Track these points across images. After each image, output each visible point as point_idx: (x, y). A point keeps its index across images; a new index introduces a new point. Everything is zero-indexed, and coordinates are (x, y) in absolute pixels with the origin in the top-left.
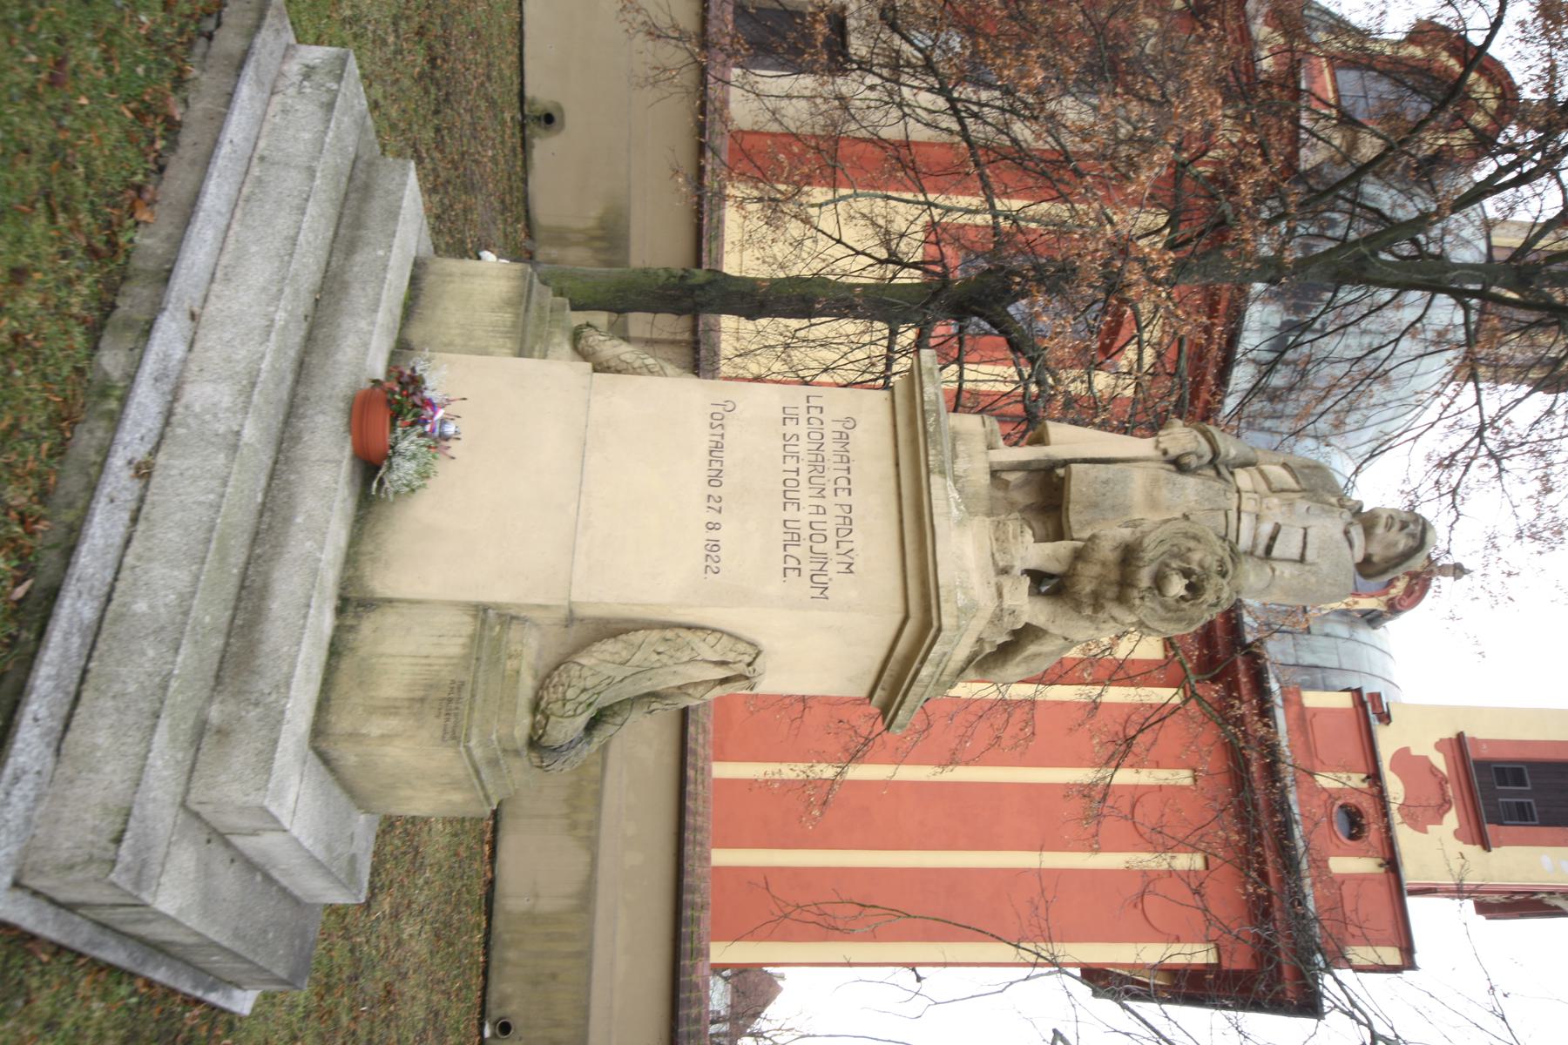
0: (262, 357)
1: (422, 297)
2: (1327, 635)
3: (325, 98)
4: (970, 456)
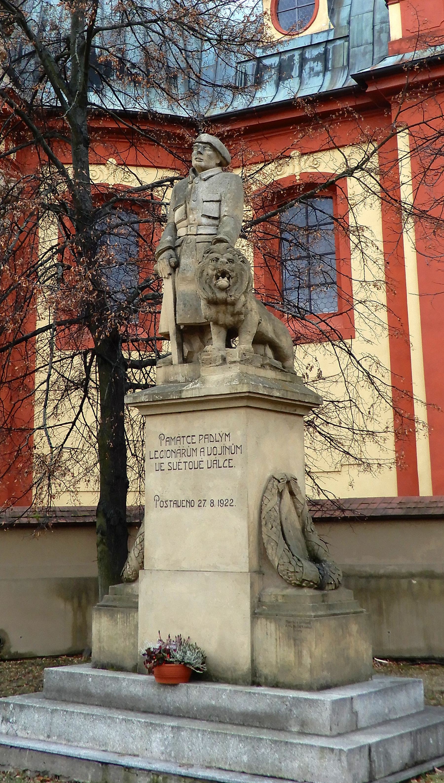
0: (139, 722)
1: (112, 662)
2: (349, 23)
3: (18, 710)
4: (176, 374)
